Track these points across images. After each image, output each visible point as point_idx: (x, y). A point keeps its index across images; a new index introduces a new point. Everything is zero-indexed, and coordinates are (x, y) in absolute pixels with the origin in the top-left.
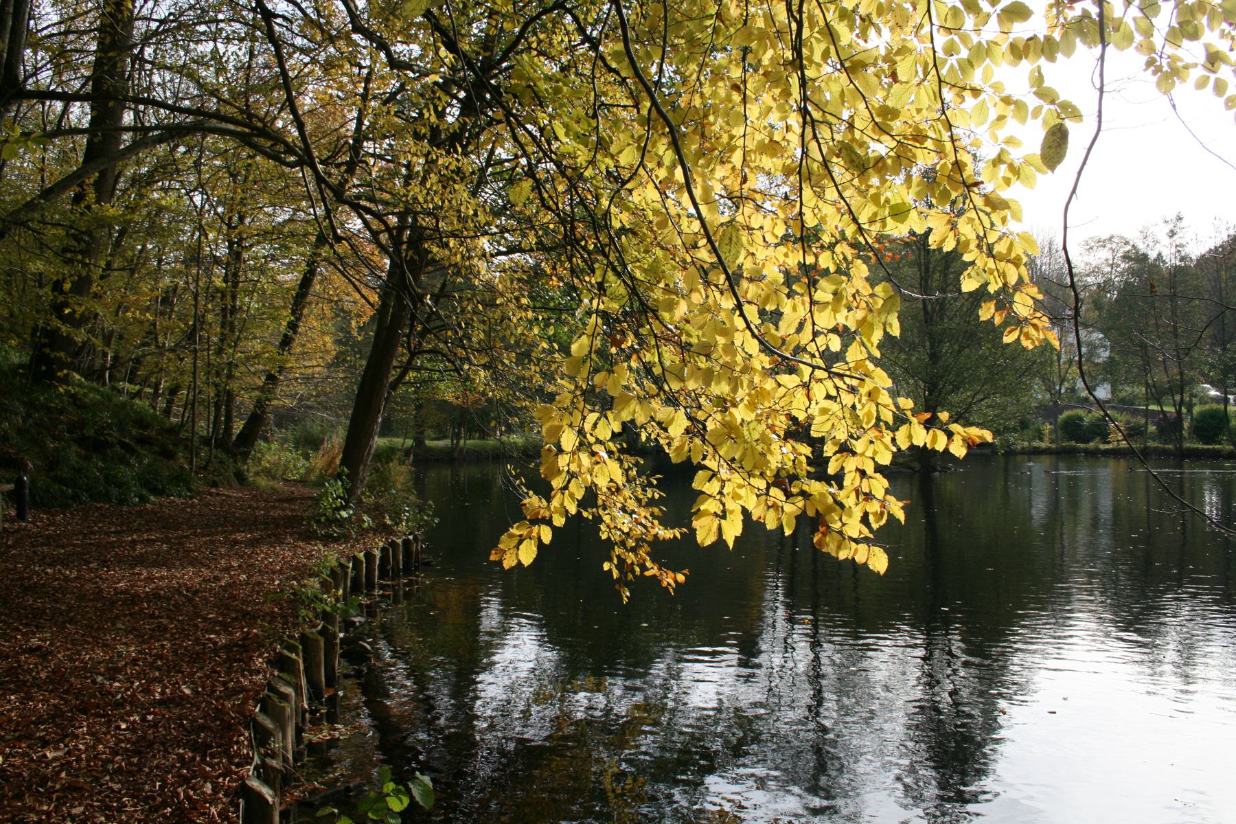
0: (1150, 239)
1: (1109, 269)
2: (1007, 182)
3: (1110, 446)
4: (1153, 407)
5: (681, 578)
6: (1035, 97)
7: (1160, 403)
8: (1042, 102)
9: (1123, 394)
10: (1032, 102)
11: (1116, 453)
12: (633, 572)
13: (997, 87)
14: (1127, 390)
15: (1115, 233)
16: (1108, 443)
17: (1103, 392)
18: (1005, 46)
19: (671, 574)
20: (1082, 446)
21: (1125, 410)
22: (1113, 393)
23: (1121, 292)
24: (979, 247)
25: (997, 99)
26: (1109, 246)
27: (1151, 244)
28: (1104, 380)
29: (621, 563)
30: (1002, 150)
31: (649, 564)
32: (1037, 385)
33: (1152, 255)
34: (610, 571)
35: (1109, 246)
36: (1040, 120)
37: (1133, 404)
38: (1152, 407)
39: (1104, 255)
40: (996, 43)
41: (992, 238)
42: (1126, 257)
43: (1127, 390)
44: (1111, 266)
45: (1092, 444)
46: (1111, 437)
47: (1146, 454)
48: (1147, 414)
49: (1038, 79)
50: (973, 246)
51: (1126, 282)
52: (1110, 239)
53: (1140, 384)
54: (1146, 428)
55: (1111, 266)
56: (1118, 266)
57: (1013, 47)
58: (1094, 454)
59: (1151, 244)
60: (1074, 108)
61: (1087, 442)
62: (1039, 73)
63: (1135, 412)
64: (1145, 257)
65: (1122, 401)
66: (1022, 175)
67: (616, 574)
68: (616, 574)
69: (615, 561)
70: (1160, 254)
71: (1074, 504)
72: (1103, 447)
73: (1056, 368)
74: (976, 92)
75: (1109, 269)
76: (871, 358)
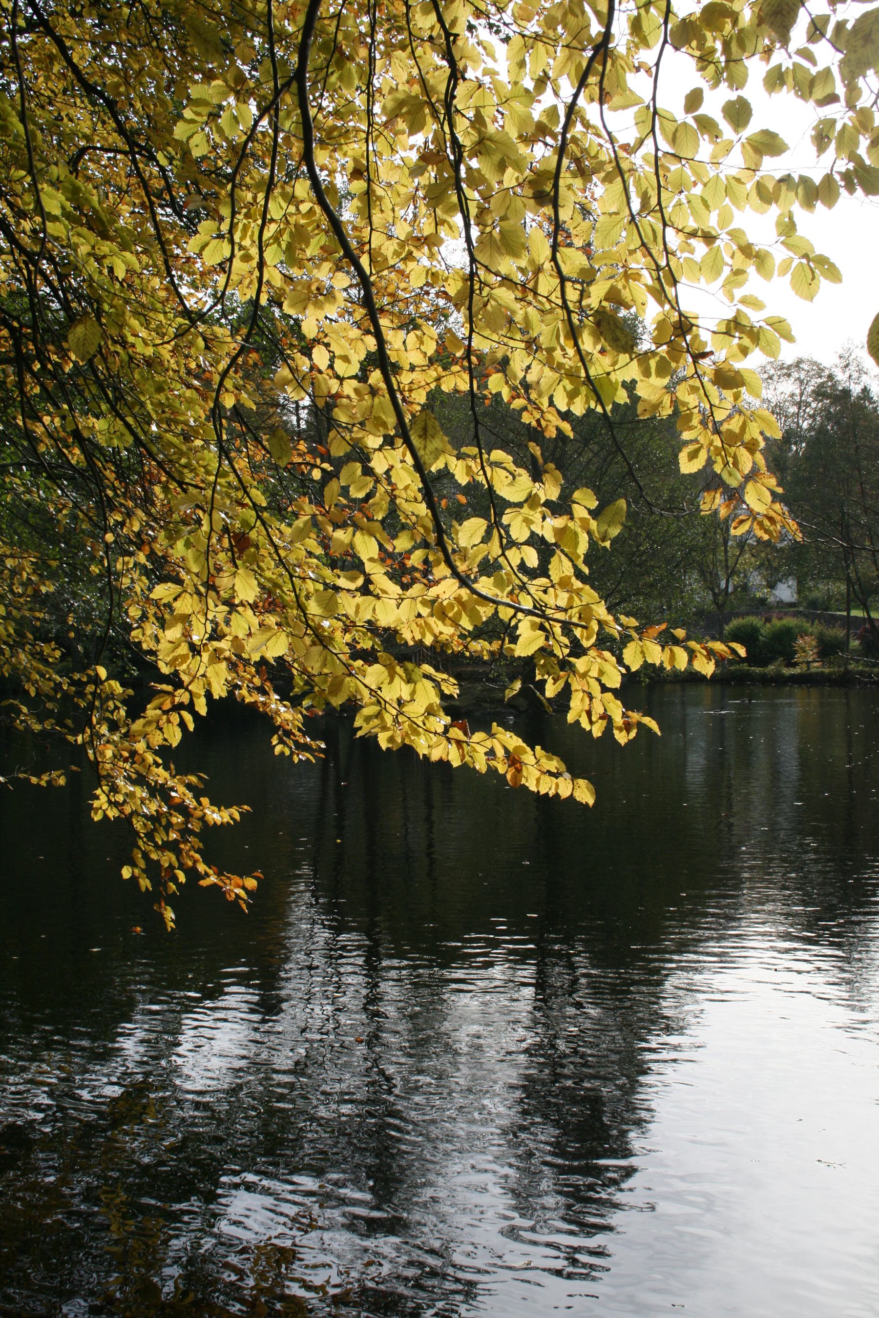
0: (852, 367)
1: (793, 409)
2: (744, 351)
3: (797, 670)
4: (856, 613)
5: (251, 883)
6: (783, 248)
7: (866, 609)
8: (791, 254)
9: (815, 594)
10: (779, 254)
11: (807, 680)
12: (175, 879)
13: (735, 235)
14: (822, 589)
15: (805, 356)
16: (795, 665)
17: (785, 592)
18: (750, 185)
19: (236, 879)
20: (757, 670)
21: (818, 617)
22: (799, 592)
23: (813, 444)
24: (704, 423)
25: (735, 247)
26: (795, 375)
27: (855, 375)
28: (786, 576)
29: (153, 869)
30: (738, 311)
31: (202, 868)
32: (693, 581)
33: (856, 390)
34: (134, 879)
35: (795, 375)
36: (788, 277)
37: (827, 609)
38: (854, 613)
39: (788, 387)
40: (738, 180)
41: (719, 416)
42: (819, 393)
43: (822, 589)
44: (799, 404)
45: (771, 667)
46: (798, 658)
47: (844, 681)
48: (849, 622)
49: (788, 227)
50: (695, 422)
51: (821, 430)
52: (798, 364)
53: (839, 579)
54: (848, 642)
55: (799, 404)
56: (808, 405)
57: (760, 188)
58: (780, 681)
59: (855, 375)
60: (832, 266)
61: (765, 664)
62: (791, 218)
63: (832, 621)
64: (846, 392)
65: (813, 604)
66: (762, 342)
67: (145, 883)
68: (145, 883)
69: (142, 864)
70: (865, 390)
71: (746, 754)
72: (787, 671)
73: (721, 557)
74: (709, 238)
75: (793, 409)
76: (579, 574)
